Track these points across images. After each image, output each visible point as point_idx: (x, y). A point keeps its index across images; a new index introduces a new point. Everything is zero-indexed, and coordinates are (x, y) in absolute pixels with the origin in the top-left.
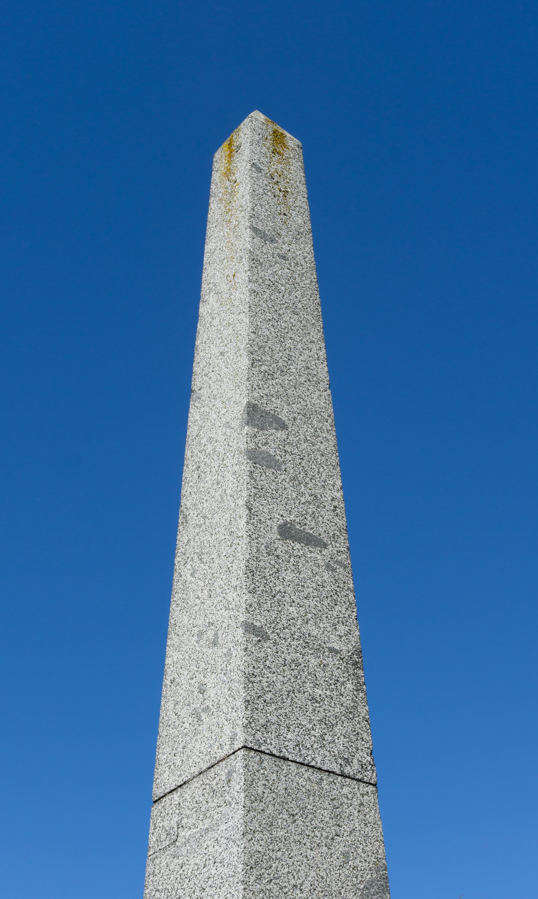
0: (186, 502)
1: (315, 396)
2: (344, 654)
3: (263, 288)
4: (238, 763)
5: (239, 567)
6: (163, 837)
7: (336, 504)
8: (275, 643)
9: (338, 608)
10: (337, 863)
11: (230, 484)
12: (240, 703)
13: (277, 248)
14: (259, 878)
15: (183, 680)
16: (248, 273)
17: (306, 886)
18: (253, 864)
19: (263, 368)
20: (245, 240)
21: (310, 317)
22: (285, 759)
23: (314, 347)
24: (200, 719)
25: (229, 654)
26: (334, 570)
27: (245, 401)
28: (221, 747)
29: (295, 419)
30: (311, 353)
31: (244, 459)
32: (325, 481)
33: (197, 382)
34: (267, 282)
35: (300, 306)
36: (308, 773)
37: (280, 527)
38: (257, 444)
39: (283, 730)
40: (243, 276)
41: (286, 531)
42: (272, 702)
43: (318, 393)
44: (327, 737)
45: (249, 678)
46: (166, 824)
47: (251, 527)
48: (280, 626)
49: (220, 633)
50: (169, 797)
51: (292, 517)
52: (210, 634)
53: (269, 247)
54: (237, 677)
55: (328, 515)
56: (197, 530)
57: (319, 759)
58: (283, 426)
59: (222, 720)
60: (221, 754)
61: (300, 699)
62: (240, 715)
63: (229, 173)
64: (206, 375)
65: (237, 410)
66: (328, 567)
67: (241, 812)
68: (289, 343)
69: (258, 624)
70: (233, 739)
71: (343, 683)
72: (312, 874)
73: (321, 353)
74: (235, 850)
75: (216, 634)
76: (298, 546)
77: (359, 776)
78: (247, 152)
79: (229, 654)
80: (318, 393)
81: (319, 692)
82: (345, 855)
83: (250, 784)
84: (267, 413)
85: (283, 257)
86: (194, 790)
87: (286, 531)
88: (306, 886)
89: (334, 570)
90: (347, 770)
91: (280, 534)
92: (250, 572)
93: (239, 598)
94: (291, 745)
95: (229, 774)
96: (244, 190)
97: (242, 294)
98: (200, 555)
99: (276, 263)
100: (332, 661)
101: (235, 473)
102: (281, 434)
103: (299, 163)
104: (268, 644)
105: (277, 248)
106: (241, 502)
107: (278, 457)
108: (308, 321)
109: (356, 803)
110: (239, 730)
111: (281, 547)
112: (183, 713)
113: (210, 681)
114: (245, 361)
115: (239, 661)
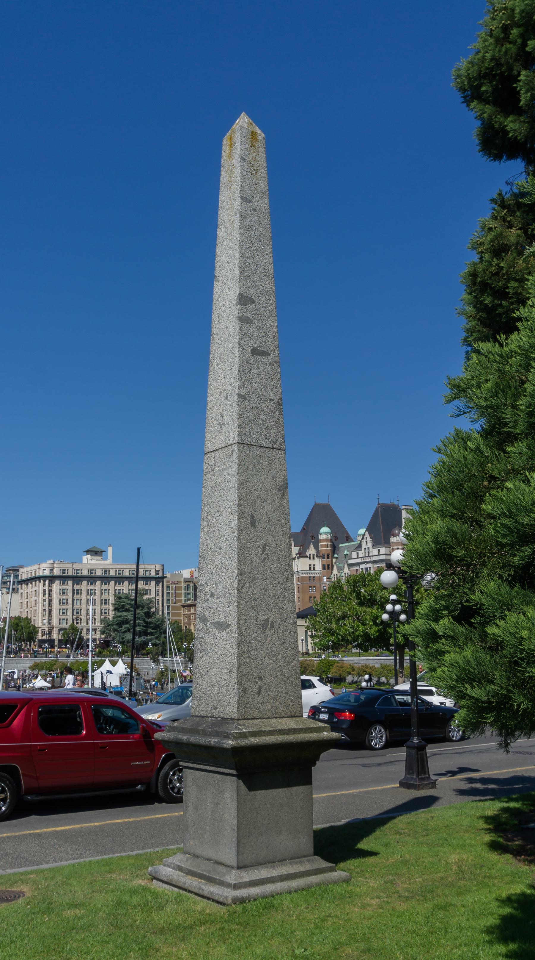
0: (214, 331)
1: (267, 283)
2: (276, 400)
3: (246, 242)
4: (236, 448)
5: (236, 369)
6: (209, 468)
7: (274, 334)
8: (249, 401)
9: (273, 382)
10: (270, 480)
11: (232, 331)
12: (236, 425)
13: (252, 206)
14: (243, 488)
15: (215, 409)
16: (239, 224)
17: (259, 490)
18: (241, 484)
19: (245, 274)
20: (237, 204)
21: (266, 241)
22: (252, 445)
23: (267, 257)
24: (221, 427)
25: (232, 405)
26: (272, 365)
27: (238, 292)
28: (229, 440)
29: (258, 297)
30: (266, 261)
31: (237, 321)
32: (270, 325)
33: (217, 272)
34: (248, 227)
35: (262, 236)
36: (260, 449)
37: (252, 350)
38: (242, 313)
39: (252, 434)
40: (237, 224)
41: (254, 352)
42: (248, 424)
43: (269, 281)
44: (268, 435)
45: (239, 416)
46: (210, 463)
47: (240, 352)
48: (251, 393)
49: (228, 395)
50: (210, 454)
51: (257, 345)
52: (225, 394)
53: (249, 207)
54: (235, 415)
55: (270, 340)
56: (219, 346)
57: (264, 444)
58: (254, 302)
59: (230, 430)
60: (229, 443)
61: (258, 421)
62: (236, 430)
63: (230, 157)
64: (221, 270)
65: (235, 296)
66: (271, 364)
67: (237, 466)
68: (257, 258)
69: (243, 394)
70: (234, 438)
71: (274, 413)
72: (261, 485)
73: (271, 260)
74: (235, 479)
75: (227, 395)
76: (259, 357)
77: (279, 448)
78: (239, 149)
79: (232, 405)
80: (269, 281)
81: (265, 417)
82: (273, 477)
83: (240, 456)
84: (247, 297)
85: (255, 210)
86: (219, 454)
87: (254, 352)
88: (259, 490)
89: (272, 365)
90: (275, 446)
91: (252, 353)
92: (239, 371)
93: (236, 383)
94: (254, 439)
95: (233, 451)
96: (237, 172)
97: (236, 234)
98: (220, 358)
99: (252, 214)
100: (270, 404)
101: (233, 326)
102: (253, 306)
103: (264, 149)
104: (247, 401)
105: (252, 206)
106: (237, 341)
107: (251, 318)
108: (265, 244)
109: (277, 458)
110: (236, 436)
111: (252, 359)
112: (215, 422)
113: (225, 413)
114: (238, 272)
115: (235, 409)
